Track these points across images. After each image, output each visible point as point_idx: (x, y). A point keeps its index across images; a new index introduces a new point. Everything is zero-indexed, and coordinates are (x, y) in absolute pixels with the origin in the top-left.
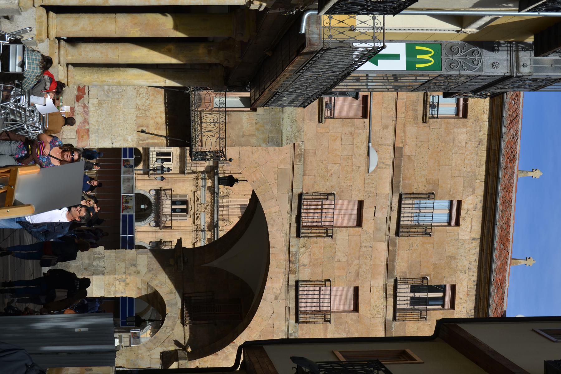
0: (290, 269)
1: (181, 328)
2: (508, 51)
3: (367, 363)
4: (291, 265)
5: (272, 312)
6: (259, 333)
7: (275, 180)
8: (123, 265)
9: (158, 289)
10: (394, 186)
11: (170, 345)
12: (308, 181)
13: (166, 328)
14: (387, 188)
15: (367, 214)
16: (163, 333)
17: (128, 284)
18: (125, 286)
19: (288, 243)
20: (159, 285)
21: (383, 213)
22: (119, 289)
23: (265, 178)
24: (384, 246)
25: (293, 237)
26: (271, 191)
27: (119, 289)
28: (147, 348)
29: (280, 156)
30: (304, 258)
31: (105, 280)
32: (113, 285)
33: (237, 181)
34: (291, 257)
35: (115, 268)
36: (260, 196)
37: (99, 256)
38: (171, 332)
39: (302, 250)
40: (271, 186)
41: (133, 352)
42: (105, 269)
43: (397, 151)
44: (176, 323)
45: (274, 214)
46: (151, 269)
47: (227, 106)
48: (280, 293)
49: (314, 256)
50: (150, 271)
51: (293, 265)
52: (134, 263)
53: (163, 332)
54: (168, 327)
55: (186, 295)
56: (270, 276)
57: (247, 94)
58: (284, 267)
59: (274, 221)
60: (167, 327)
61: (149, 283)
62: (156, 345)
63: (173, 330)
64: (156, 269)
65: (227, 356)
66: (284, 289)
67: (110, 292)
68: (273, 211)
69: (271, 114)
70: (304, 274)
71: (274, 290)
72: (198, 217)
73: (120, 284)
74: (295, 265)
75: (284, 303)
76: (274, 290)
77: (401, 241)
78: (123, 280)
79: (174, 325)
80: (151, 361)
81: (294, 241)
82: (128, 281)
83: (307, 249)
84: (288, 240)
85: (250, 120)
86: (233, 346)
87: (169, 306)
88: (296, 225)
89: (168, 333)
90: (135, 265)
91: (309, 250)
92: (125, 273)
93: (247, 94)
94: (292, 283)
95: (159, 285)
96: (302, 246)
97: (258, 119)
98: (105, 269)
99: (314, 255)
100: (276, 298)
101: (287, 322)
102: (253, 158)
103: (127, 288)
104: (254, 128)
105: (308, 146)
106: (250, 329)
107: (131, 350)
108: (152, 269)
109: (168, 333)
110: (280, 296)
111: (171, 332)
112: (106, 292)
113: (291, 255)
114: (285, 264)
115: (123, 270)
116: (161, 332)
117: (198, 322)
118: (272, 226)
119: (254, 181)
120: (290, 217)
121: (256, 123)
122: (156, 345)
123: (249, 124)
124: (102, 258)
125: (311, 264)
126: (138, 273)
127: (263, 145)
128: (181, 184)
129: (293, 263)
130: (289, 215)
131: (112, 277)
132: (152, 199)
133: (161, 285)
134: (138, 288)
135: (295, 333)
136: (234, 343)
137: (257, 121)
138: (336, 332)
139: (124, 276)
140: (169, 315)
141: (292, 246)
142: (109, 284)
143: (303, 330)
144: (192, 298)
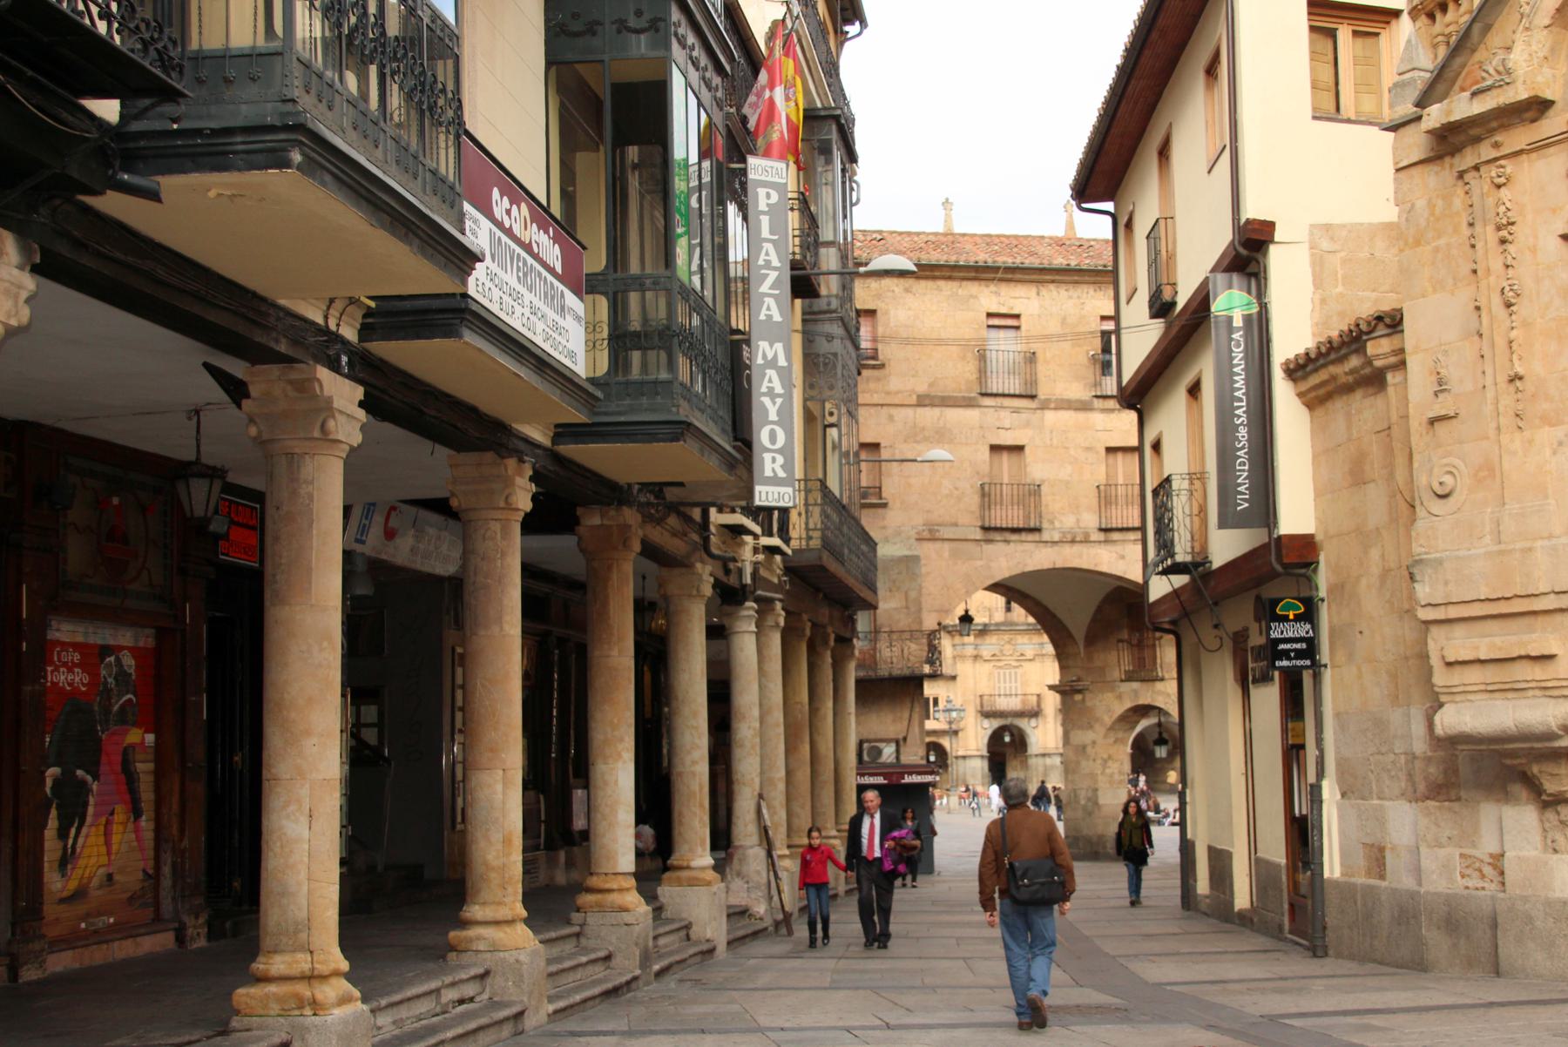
8: (1084, 763)
10: (969, 403)
12: (965, 519)
30: (1068, 522)
33: (967, 611)
55: (1123, 677)
66: (1110, 547)
72: (1022, 655)
77: (1043, 393)
82: (1105, 756)
83: (1055, 518)
90: (1084, 747)
92: (1094, 760)
94: (1101, 536)
100: (1123, 557)
105: (919, 520)
114: (1076, 548)
115: (1091, 762)
118: (1025, 565)
120: (1014, 541)
134: (1115, 742)
139: (1099, 762)
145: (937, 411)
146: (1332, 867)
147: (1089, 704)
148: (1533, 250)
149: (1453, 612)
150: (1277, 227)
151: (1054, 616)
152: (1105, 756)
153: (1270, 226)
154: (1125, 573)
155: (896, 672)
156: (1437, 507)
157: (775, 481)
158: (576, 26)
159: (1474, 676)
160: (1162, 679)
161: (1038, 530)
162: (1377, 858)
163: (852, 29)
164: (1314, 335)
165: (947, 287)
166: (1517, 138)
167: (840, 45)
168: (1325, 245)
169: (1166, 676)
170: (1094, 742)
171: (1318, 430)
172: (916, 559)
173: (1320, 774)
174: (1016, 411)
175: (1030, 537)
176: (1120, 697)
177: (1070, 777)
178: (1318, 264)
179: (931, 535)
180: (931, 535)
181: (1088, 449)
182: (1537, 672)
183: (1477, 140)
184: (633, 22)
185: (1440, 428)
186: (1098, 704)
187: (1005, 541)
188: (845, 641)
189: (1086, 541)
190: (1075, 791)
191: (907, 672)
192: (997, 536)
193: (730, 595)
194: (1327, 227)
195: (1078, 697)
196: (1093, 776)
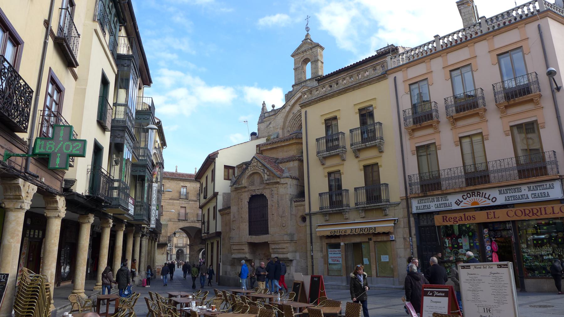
2: (429, 172)
3: (448, 290)
10: (178, 200)
12: (176, 218)
14: (178, 202)
15: (183, 206)
21: (183, 202)
24: (190, 202)
30: (192, 219)
43: (170, 199)
57: (130, 160)
70: (195, 219)
77: (189, 198)
81: (188, 221)
93: (130, 160)
105: (168, 218)
114: (193, 223)
128: (174, 242)
132: (178, 249)
145: (172, 201)
146: (221, 274)
148: (244, 203)
149: (234, 244)
150: (291, 54)
153: (218, 193)
155: (163, 243)
156: (233, 231)
157: (153, 224)
158: (134, 171)
159: (236, 251)
162: (226, 272)
163: (165, 147)
164: (312, 74)
165: (176, 182)
166: (243, 190)
167: (162, 149)
168: (225, 195)
171: (222, 218)
172: (167, 224)
173: (220, 262)
174: (185, 201)
175: (186, 221)
176: (199, 247)
178: (223, 197)
179: (170, 220)
180: (170, 220)
181: (196, 208)
182: (242, 251)
183: (239, 189)
184: (141, 171)
185: (234, 222)
188: (156, 239)
189: (195, 222)
191: (164, 243)
192: (180, 221)
193: (143, 236)
194: (225, 193)
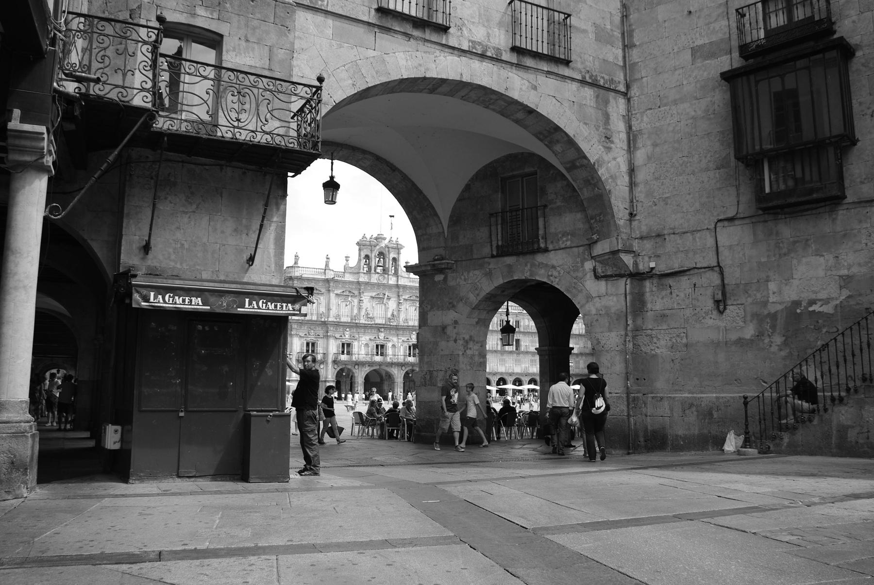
0: (494, 56)
1: (552, 255)
4: (489, 54)
5: (554, 99)
6: (581, 124)
7: (352, 49)
8: (443, 344)
9: (483, 294)
11: (581, 269)
13: (552, 276)
16: (560, 280)
17: (471, 337)
18: (474, 341)
19: (456, 52)
20: (477, 292)
22: (477, 350)
23: (349, 65)
25: (447, 40)
26: (372, 60)
27: (477, 350)
28: (587, 302)
29: (311, 31)
30: (479, 34)
31: (465, 369)
32: (471, 358)
33: (332, 177)
34: (476, 50)
35: (447, 355)
36: (380, 78)
37: (428, 377)
38: (559, 269)
39: (465, 32)
40: (362, 57)
41: (595, 323)
42: (449, 368)
44: (543, 263)
45: (410, 63)
46: (451, 305)
47: (206, 100)
48: (528, 81)
49: (474, 18)
50: (454, 306)
51: (489, 50)
52: (439, 329)
53: (557, 280)
54: (550, 273)
55: (495, 253)
56: (504, 90)
58: (490, 65)
59: (420, 65)
60: (548, 275)
61: (474, 306)
62: (582, 290)
63: (554, 267)
64: (451, 299)
65: (611, 177)
66: (521, 73)
67: (481, 362)
68: (405, 63)
69: (230, 10)
71: (524, 88)
72: (318, 335)
73: (470, 349)
74: (489, 48)
75: (542, 79)
76: (524, 88)
78: (465, 344)
79: (547, 265)
80: (612, 295)
82: (467, 337)
83: (464, 24)
84: (451, 51)
85: (240, 49)
86: (598, 166)
87: (512, 276)
88: (428, 31)
89: (559, 273)
90: (444, 328)
91: (466, 22)
92: (455, 341)
94: (514, 58)
95: (477, 292)
96: (460, 31)
97: (239, 36)
98: (449, 368)
99: (473, 17)
100: (535, 88)
101: (567, 80)
102: (312, 78)
103: (476, 339)
104: (256, 46)
106: (576, 135)
107: (591, 326)
108: (450, 303)
109: (559, 273)
110: (531, 81)
111: (559, 269)
112: (480, 369)
113: (474, 51)
115: (451, 343)
116: (557, 284)
117: (541, 232)
118: (427, 69)
119: (353, 85)
120: (416, 38)
121: (247, 41)
122: (582, 290)
123: (247, 54)
124: (432, 374)
125: (486, 24)
126: (456, 322)
127: (291, 37)
129: (486, 50)
130: (412, 40)
131: (461, 359)
133: (476, 289)
134: (477, 323)
135: (581, 72)
136: (594, 163)
137: (243, 38)
138: (579, 15)
139: (461, 342)
140: (528, 274)
141: (460, 44)
142: (471, 364)
143: (577, 61)
144: (500, 243)
147: (451, 283)
151: (421, 192)
152: (467, 337)
154: (537, 106)
160: (546, 250)
161: (444, 29)
169: (551, 247)
170: (456, 322)
176: (489, 275)
177: (426, 359)
186: (462, 283)
187: (405, 34)
190: (431, 372)
195: (439, 278)
196: (453, 357)
